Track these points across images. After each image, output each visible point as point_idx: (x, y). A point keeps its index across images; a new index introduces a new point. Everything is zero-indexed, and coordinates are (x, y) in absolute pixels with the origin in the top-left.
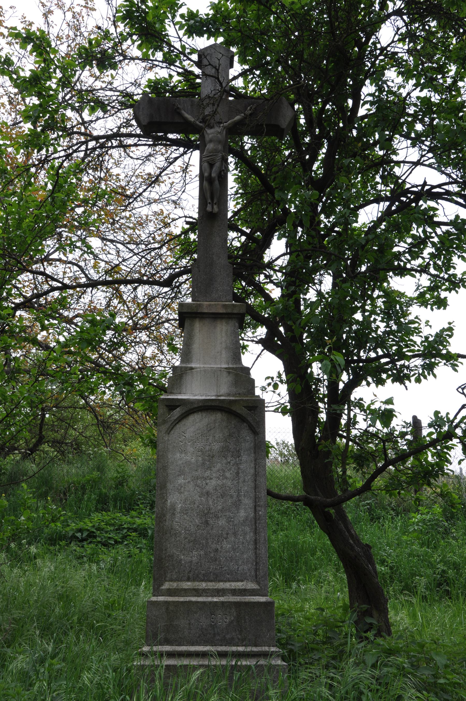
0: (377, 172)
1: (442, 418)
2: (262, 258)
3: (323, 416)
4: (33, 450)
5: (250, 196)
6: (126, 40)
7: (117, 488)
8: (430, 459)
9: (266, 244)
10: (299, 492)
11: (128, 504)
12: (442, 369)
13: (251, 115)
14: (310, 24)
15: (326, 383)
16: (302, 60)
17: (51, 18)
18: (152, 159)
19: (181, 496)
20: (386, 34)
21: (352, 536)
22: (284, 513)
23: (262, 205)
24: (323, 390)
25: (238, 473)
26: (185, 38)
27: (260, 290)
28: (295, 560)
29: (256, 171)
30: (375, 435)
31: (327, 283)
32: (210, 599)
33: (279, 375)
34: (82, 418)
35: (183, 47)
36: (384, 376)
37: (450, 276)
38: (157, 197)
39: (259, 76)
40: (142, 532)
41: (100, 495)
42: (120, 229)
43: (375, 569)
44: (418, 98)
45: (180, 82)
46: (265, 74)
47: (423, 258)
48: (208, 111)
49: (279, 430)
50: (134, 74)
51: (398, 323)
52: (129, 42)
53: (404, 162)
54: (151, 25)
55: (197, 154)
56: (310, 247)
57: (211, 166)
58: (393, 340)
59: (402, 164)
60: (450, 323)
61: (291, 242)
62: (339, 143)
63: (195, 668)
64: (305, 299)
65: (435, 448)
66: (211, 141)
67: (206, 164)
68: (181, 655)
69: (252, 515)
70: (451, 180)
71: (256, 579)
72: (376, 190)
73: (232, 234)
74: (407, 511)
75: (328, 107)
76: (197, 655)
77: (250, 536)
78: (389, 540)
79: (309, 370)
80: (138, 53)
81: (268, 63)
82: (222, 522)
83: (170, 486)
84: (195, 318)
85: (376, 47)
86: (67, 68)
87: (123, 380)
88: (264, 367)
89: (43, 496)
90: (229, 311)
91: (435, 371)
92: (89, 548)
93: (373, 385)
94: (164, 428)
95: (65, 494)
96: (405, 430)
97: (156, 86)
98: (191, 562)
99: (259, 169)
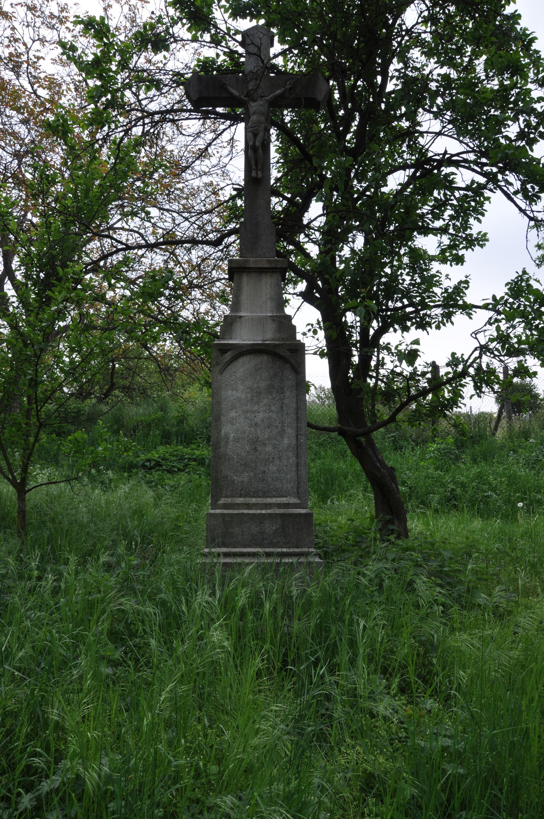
0: (404, 142)
1: (457, 359)
2: (302, 220)
3: (356, 359)
4: (106, 395)
5: (290, 164)
6: (177, 23)
7: (178, 425)
8: (446, 395)
9: (305, 207)
10: (335, 424)
11: (188, 439)
12: (459, 317)
13: (290, 88)
14: (343, 7)
15: (358, 329)
16: (335, 39)
17: (110, 12)
18: (202, 135)
19: (234, 427)
20: (411, 16)
21: (379, 461)
22: (321, 445)
23: (301, 172)
24: (356, 337)
25: (282, 407)
26: (230, 21)
27: (300, 250)
28: (330, 483)
29: (296, 141)
30: (401, 374)
31: (359, 242)
32: (259, 511)
33: (319, 323)
34: (147, 368)
35: (228, 29)
36: (409, 324)
37: (467, 235)
38: (207, 170)
39: (297, 55)
40: (201, 461)
41: (164, 431)
42: (175, 200)
43: (398, 489)
44: (439, 75)
45: (225, 61)
46: (303, 53)
47: (444, 220)
48: (251, 86)
49: (318, 372)
50: (185, 55)
51: (422, 277)
52: (180, 25)
53: (427, 132)
54: (199, 10)
55: (242, 126)
56: (345, 208)
57: (255, 135)
58: (417, 292)
59: (425, 135)
60: (467, 277)
61: (327, 204)
62: (371, 116)
63: (248, 564)
64: (339, 256)
65: (451, 386)
66: (254, 113)
67: (250, 134)
68: (235, 555)
69: (294, 442)
70: (468, 149)
71: (298, 495)
72: (402, 158)
73: (274, 200)
74: (425, 442)
75: (359, 83)
76: (249, 555)
77: (293, 460)
78: (410, 466)
79: (343, 319)
80: (189, 36)
81: (305, 43)
82: (269, 449)
83: (223, 419)
84: (243, 272)
85: (401, 28)
86: (126, 53)
87: (182, 331)
88: (304, 316)
89: (116, 432)
90: (273, 265)
91: (453, 319)
92: (156, 475)
93: (399, 331)
94: (217, 369)
95: (134, 431)
96: (426, 370)
97: (206, 65)
98: (243, 482)
99: (298, 139)
